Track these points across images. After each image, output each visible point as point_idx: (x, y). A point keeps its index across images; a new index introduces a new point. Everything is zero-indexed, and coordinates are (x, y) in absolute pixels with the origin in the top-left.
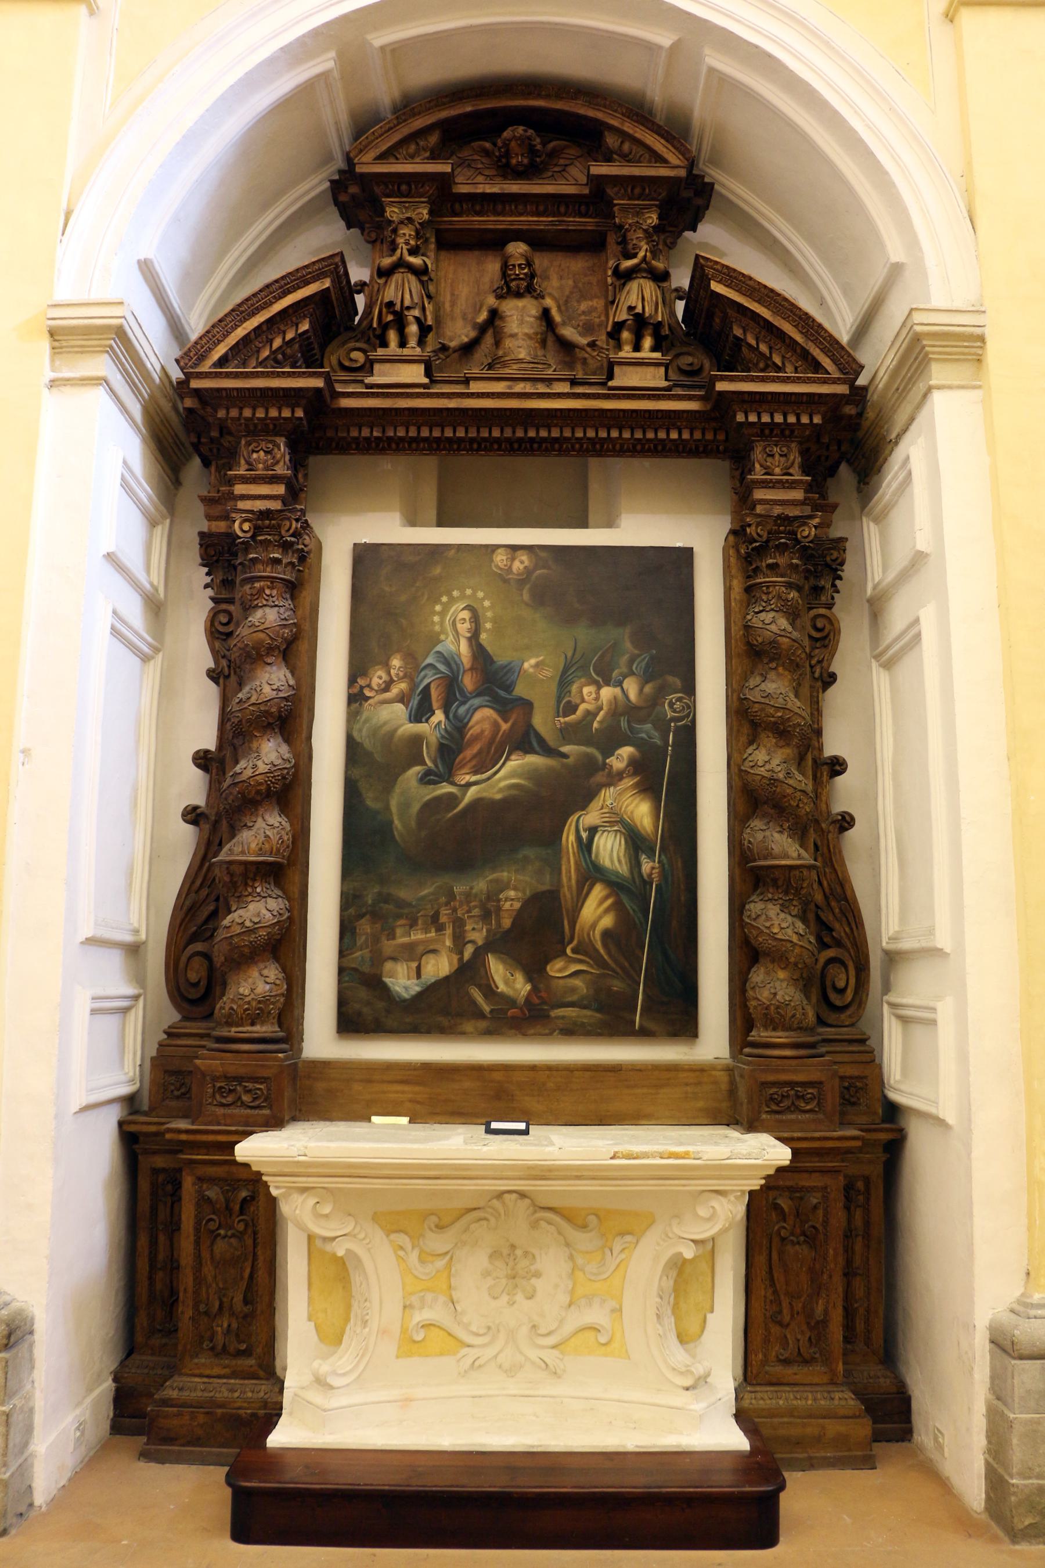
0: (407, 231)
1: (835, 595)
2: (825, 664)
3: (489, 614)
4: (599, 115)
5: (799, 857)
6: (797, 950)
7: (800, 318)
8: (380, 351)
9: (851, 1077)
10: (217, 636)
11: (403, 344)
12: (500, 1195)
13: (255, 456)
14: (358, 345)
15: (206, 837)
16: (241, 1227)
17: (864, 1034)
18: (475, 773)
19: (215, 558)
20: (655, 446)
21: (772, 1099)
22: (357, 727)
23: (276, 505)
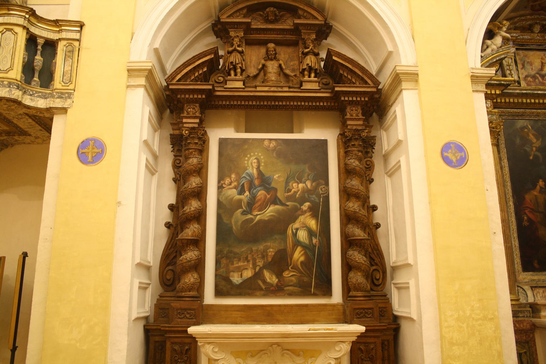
0: (237, 40)
1: (373, 154)
2: (370, 176)
3: (263, 161)
4: (297, 4)
5: (364, 236)
6: (364, 266)
7: (361, 67)
8: (229, 77)
9: (382, 307)
10: (176, 167)
11: (236, 75)
12: (272, 344)
13: (189, 110)
14: (221, 75)
15: (173, 232)
16: (186, 358)
17: (386, 293)
18: (259, 211)
19: (175, 142)
20: (316, 107)
21: (357, 314)
22: (221, 197)
23: (196, 126)
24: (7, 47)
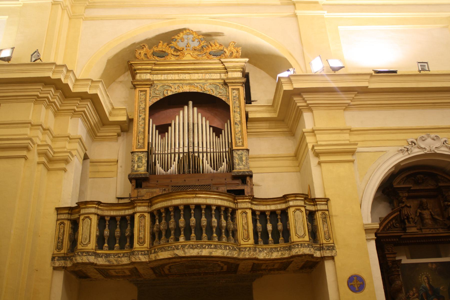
3: (431, 278)
24: (299, 221)
